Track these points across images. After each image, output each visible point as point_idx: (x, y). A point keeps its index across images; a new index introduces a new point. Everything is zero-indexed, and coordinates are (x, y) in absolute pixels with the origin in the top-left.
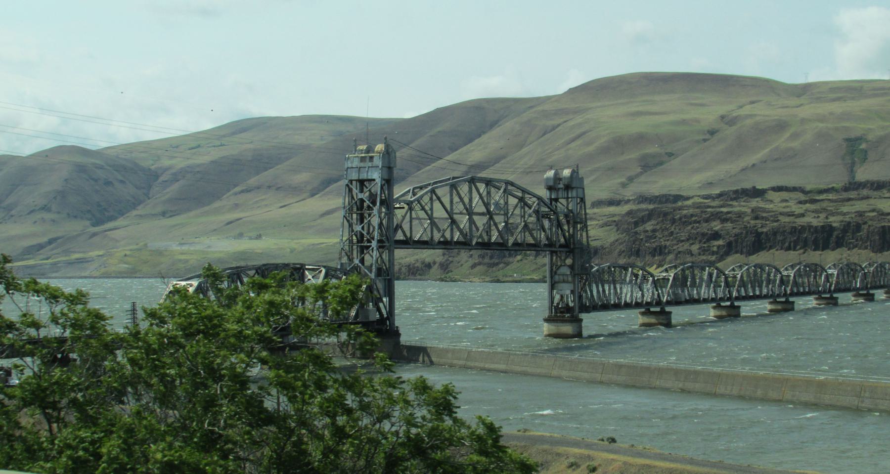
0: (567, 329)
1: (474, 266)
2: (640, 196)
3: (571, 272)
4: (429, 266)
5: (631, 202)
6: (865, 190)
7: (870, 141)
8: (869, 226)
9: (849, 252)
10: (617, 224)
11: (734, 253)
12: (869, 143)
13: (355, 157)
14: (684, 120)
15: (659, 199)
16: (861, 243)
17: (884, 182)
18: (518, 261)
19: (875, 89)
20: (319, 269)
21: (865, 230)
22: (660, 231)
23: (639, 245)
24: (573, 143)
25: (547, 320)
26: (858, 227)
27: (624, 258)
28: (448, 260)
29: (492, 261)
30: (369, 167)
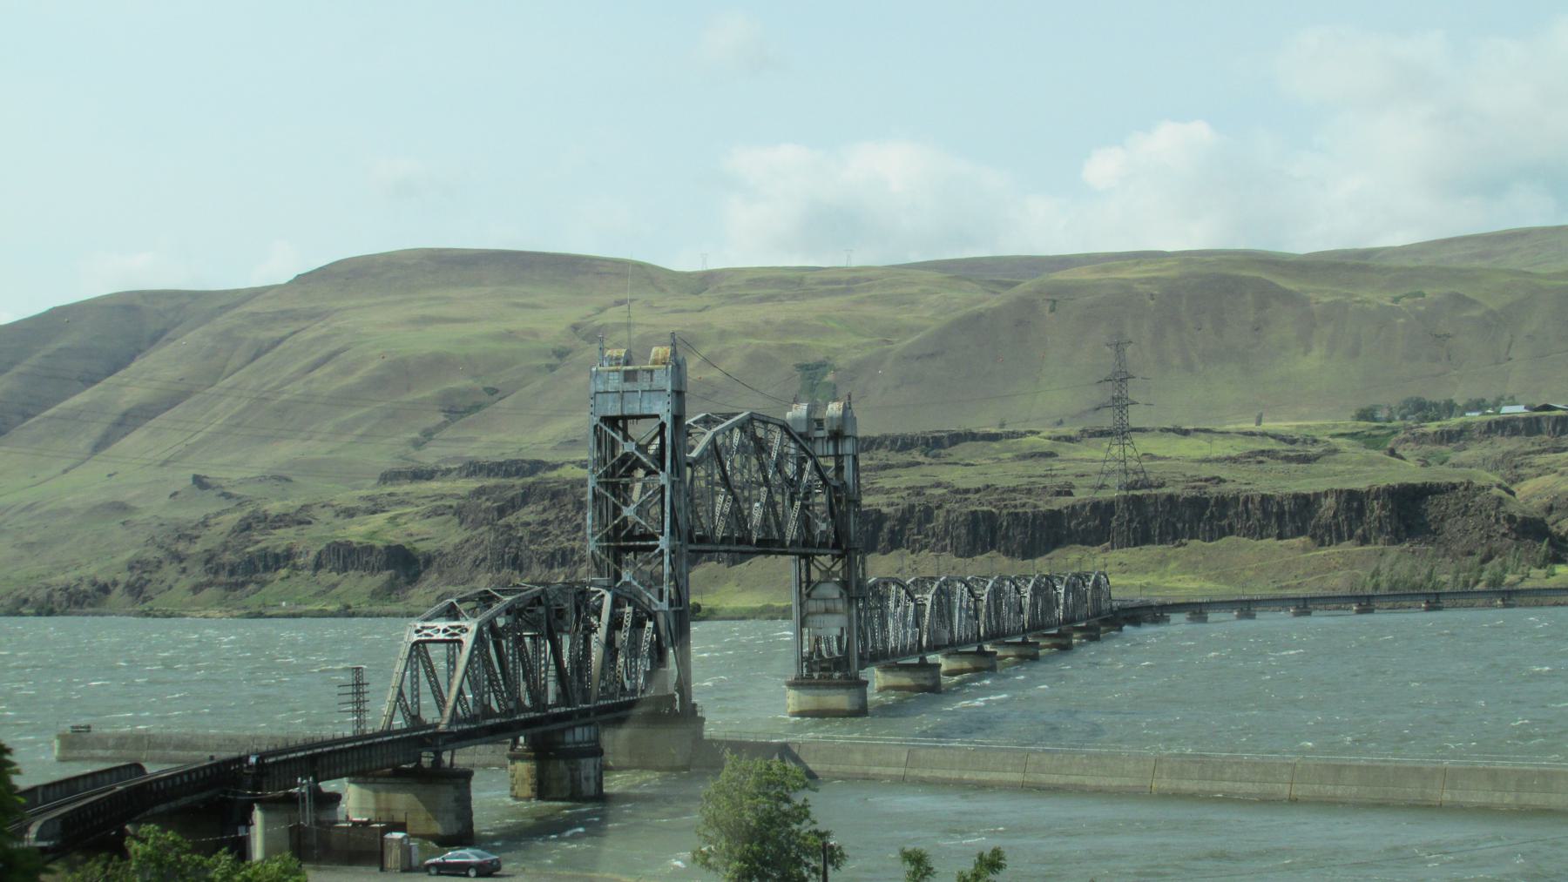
0: (839, 699)
1: (197, 589)
2: (471, 463)
3: (841, 595)
4: (105, 589)
5: (454, 473)
6: (881, 450)
7: (839, 369)
8: (948, 511)
9: (913, 556)
10: (458, 512)
11: (705, 561)
12: (839, 372)
13: (613, 371)
14: (511, 332)
15: (504, 468)
16: (934, 540)
17: (912, 437)
18: (282, 579)
19: (824, 283)
20: (599, 592)
21: (941, 519)
22: (557, 523)
23: (518, 548)
24: (317, 370)
25: (796, 684)
26: (928, 514)
27: (488, 572)
28: (142, 578)
29: (233, 580)
30: (643, 391)
